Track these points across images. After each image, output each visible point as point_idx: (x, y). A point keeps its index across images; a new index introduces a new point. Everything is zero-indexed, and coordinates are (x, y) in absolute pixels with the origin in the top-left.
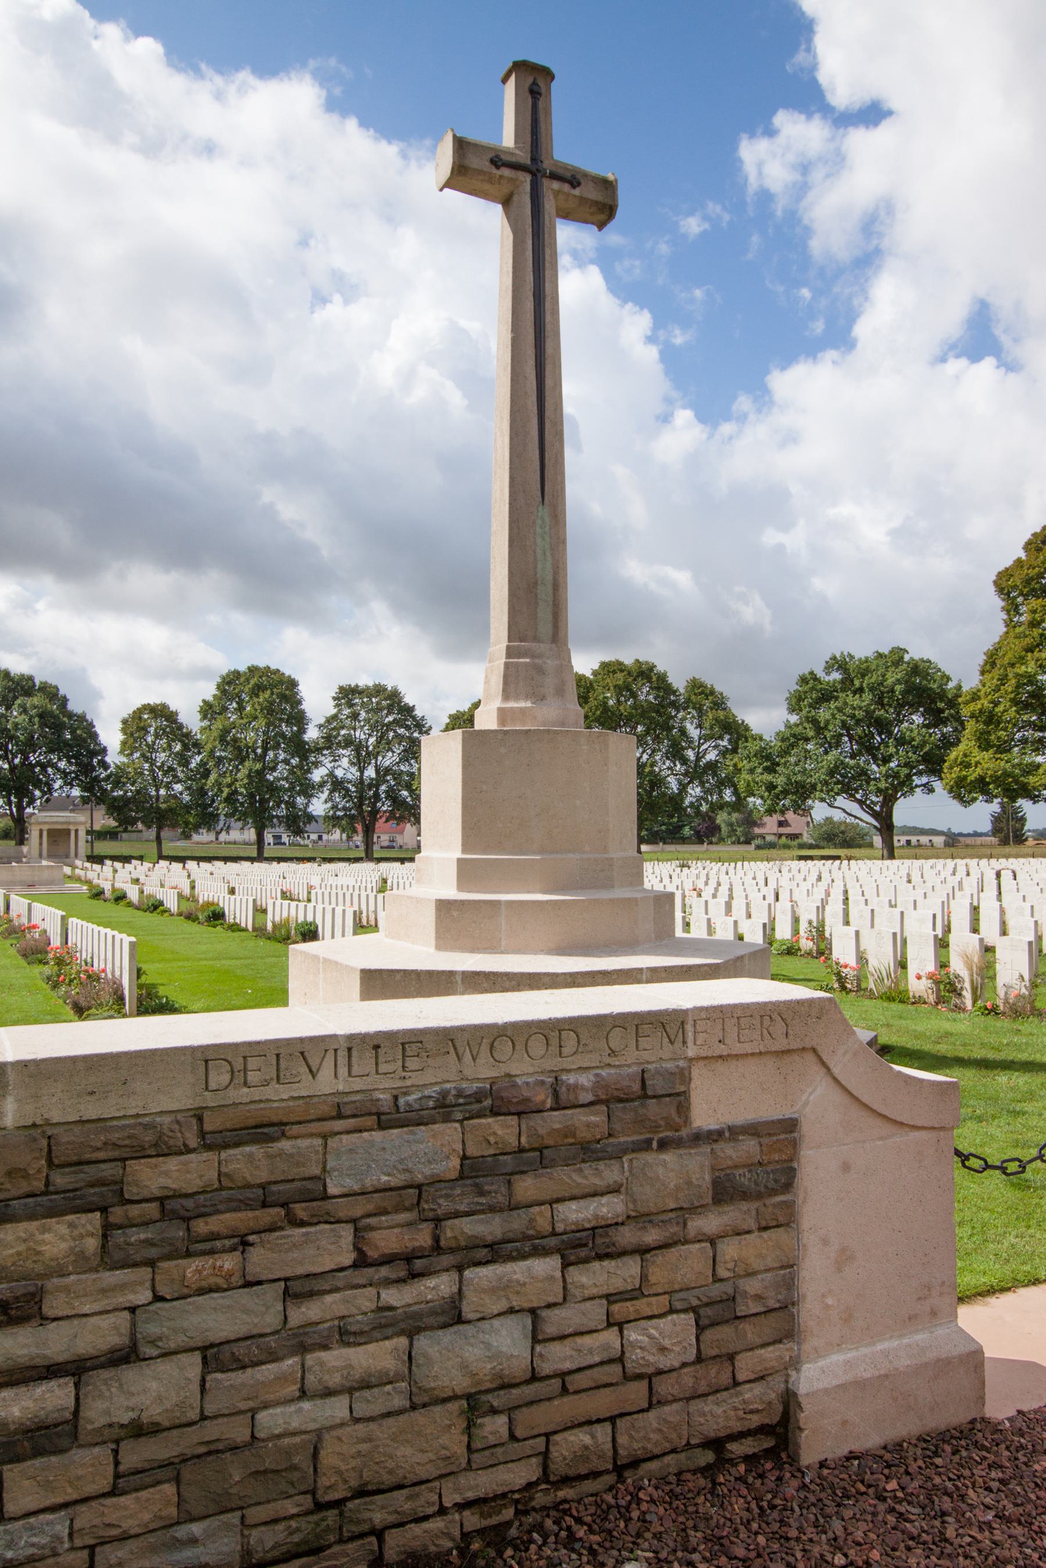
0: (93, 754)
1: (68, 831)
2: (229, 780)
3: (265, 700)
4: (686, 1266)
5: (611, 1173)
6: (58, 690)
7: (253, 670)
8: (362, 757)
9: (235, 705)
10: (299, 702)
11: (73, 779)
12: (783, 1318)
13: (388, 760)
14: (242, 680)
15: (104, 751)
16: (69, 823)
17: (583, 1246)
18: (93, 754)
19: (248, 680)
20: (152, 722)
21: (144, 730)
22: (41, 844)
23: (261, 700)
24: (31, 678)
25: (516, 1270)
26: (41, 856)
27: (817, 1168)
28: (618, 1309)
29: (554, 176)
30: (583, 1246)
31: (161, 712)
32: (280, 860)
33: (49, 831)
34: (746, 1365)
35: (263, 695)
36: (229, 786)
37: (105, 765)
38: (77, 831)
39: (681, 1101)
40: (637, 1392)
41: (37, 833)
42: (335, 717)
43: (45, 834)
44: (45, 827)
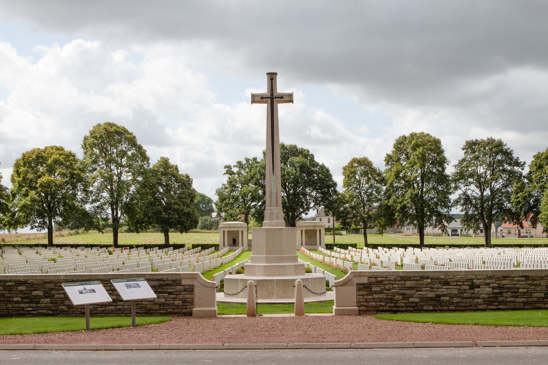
0: (329, 187)
1: (316, 231)
2: (400, 200)
3: (420, 153)
4: (181, 296)
5: (173, 287)
6: (308, 152)
7: (413, 135)
8: (481, 184)
9: (404, 156)
10: (442, 152)
11: (320, 201)
12: (192, 303)
13: (497, 185)
14: (407, 141)
15: (335, 185)
16: (316, 226)
17: (170, 293)
18: (329, 187)
19: (410, 142)
20: (360, 168)
21: (355, 173)
22: (302, 238)
23: (418, 153)
24: (295, 147)
25: (164, 295)
26: (302, 244)
27: (196, 290)
28: (174, 299)
29: (276, 98)
30: (170, 293)
31: (364, 162)
32: (434, 246)
33: (306, 231)
34: (188, 307)
35: (423, 150)
36: (401, 203)
37: (335, 192)
38: (320, 231)
39: (181, 281)
40: (176, 307)
41: (300, 232)
42: (464, 160)
43: (304, 232)
44: (304, 229)
